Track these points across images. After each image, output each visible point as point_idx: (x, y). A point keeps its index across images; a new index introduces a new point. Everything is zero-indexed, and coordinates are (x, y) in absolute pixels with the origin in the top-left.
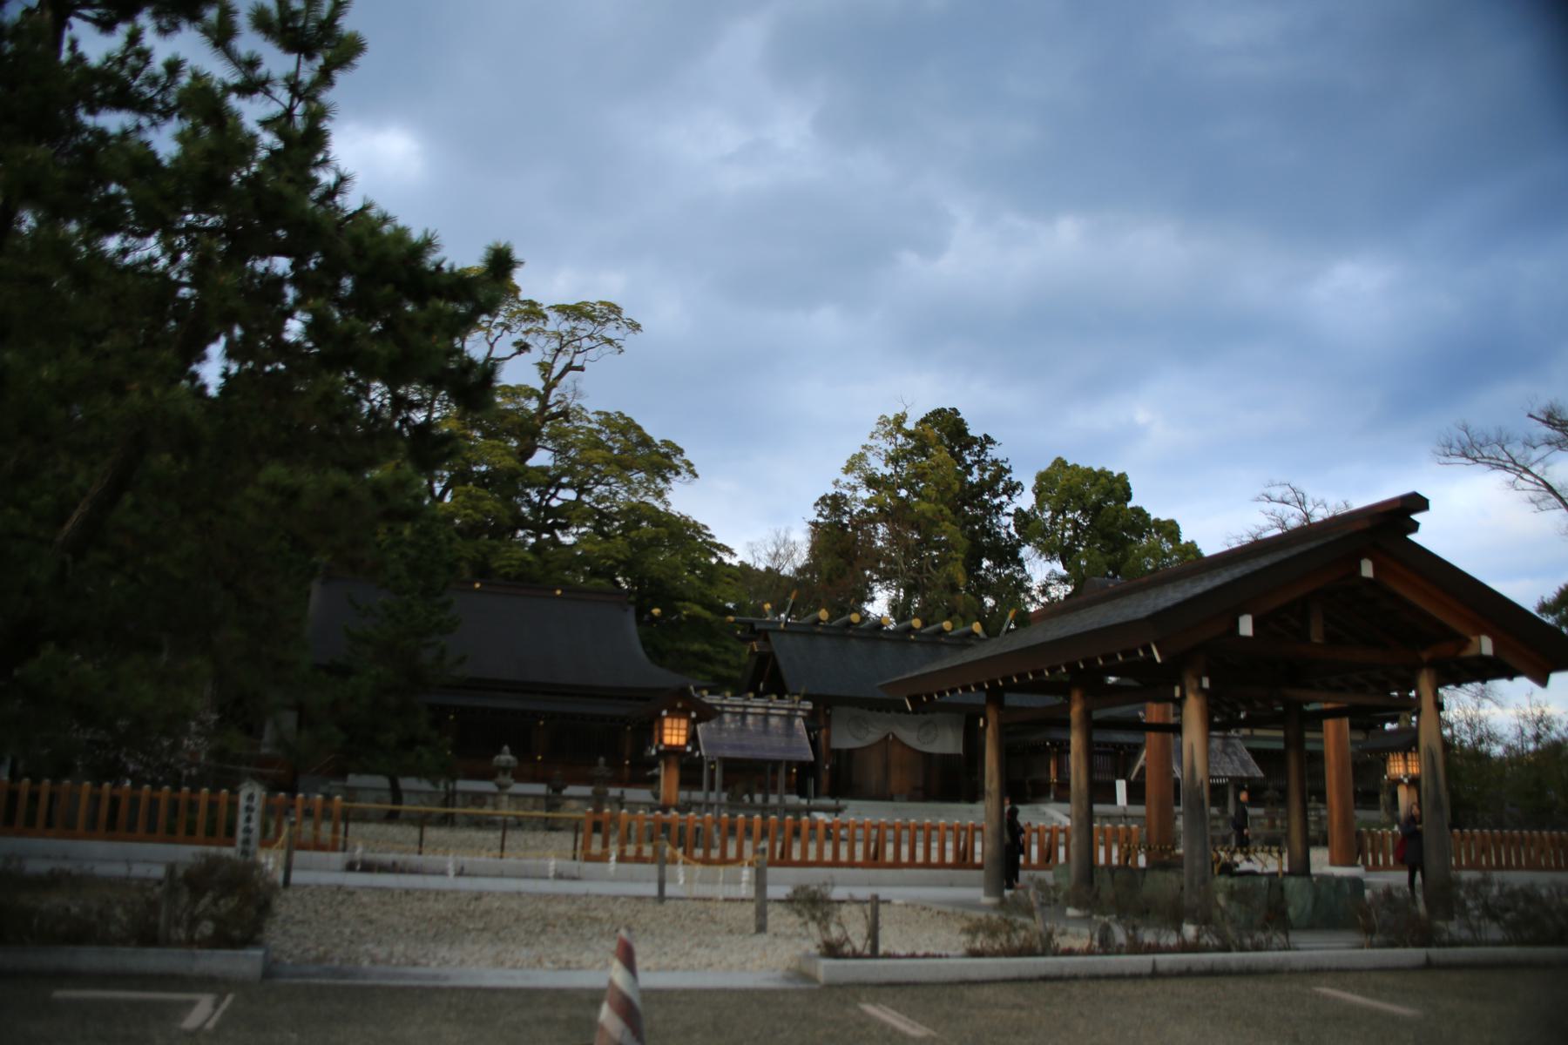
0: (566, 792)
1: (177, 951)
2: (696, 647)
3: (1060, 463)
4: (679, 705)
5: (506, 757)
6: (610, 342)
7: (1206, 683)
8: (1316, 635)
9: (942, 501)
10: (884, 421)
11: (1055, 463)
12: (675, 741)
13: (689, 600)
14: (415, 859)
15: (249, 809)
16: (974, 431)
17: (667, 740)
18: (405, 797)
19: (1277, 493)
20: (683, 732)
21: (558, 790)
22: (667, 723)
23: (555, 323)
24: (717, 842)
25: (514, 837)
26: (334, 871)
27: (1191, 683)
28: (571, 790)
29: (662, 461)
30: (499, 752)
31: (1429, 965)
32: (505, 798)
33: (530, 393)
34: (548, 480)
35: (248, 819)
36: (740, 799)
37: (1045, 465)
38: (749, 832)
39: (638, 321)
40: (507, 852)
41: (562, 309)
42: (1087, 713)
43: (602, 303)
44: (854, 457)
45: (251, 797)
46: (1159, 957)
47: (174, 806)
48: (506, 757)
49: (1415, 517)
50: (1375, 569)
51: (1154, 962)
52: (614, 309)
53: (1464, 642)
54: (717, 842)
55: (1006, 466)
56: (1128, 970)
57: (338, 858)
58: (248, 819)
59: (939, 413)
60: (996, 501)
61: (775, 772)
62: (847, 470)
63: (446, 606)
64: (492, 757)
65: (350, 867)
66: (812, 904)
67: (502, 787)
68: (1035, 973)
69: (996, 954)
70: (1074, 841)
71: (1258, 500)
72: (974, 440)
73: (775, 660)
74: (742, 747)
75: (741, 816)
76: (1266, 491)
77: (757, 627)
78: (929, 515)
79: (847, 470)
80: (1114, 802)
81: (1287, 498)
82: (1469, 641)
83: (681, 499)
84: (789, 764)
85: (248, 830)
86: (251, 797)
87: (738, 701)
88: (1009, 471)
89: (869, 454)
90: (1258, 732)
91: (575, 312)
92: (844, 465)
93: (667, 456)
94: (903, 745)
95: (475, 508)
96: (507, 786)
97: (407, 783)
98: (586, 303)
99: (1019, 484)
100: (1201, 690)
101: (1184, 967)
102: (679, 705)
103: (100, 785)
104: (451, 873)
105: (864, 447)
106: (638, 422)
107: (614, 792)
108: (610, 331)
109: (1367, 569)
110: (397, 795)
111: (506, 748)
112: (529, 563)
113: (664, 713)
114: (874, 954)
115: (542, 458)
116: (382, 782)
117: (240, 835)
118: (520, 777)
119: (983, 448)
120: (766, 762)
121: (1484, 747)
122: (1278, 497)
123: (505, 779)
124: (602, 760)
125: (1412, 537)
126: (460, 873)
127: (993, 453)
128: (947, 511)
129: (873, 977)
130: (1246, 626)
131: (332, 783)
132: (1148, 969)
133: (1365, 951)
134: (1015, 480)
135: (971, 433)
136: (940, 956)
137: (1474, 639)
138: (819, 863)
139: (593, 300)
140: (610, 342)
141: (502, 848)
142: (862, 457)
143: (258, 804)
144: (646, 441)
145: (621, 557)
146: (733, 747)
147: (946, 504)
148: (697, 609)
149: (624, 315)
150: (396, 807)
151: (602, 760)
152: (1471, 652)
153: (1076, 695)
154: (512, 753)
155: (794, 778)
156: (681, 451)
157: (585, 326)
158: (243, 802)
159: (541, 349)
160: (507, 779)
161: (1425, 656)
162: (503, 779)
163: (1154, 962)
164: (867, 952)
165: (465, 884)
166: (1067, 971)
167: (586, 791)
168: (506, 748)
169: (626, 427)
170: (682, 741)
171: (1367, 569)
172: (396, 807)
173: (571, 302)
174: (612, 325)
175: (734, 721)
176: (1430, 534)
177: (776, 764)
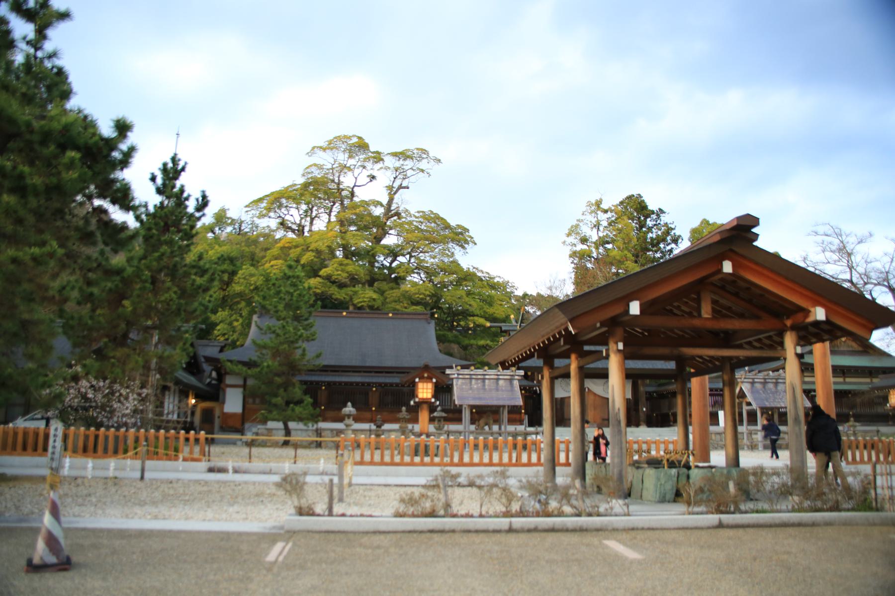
2: (482, 343)
3: (705, 222)
4: (426, 375)
5: (349, 409)
6: (423, 171)
7: (621, 346)
8: (706, 311)
9: (627, 248)
10: (590, 204)
11: (702, 223)
12: (425, 396)
13: (477, 316)
14: (246, 465)
15: (55, 436)
16: (652, 206)
17: (421, 395)
18: (293, 433)
19: (821, 230)
20: (430, 391)
21: (379, 426)
22: (420, 385)
23: (390, 161)
24: (449, 452)
25: (300, 452)
26: (201, 472)
27: (612, 346)
28: (386, 426)
29: (460, 237)
30: (345, 406)
31: (721, 525)
32: (350, 432)
33: (378, 203)
34: (393, 253)
35: (55, 441)
36: (483, 428)
37: (696, 224)
38: (476, 446)
39: (439, 158)
40: (253, 459)
41: (395, 155)
42: (581, 368)
43: (417, 149)
44: (572, 227)
45: (56, 430)
46: (514, 520)
47: (117, 438)
48: (349, 409)
49: (754, 230)
50: (734, 266)
51: (511, 523)
52: (424, 151)
53: (807, 312)
54: (449, 452)
55: (673, 226)
56: (491, 528)
57: (203, 465)
58: (55, 441)
59: (630, 197)
60: (668, 248)
62: (569, 235)
63: (311, 326)
64: (341, 409)
65: (211, 470)
66: (292, 484)
67: (347, 426)
68: (425, 528)
69: (413, 516)
70: (571, 447)
71: (809, 235)
72: (653, 212)
74: (480, 399)
75: (481, 438)
76: (814, 229)
77: (503, 329)
78: (618, 258)
79: (569, 235)
80: (718, 424)
81: (829, 233)
82: (810, 311)
83: (466, 259)
85: (54, 447)
86: (56, 430)
87: (480, 372)
88: (673, 229)
89: (581, 224)
90: (848, 380)
91: (403, 155)
92: (567, 232)
93: (461, 233)
94: (595, 394)
95: (343, 271)
96: (350, 425)
97: (292, 425)
98: (408, 150)
99: (679, 236)
100: (619, 351)
101: (532, 526)
102: (426, 375)
103: (79, 429)
104: (231, 471)
105: (578, 220)
106: (441, 215)
107: (410, 426)
108: (423, 165)
109: (727, 267)
110: (288, 432)
111: (349, 404)
112: (374, 300)
114: (331, 514)
115: (390, 240)
116: (280, 425)
117: (50, 449)
118: (357, 419)
119: (658, 216)
121: (184, 366)
122: (822, 233)
125: (755, 244)
126: (236, 471)
127: (664, 219)
128: (629, 255)
129: (317, 528)
130: (635, 308)
131: (259, 427)
132: (506, 527)
133: (686, 517)
134: (677, 234)
135: (650, 208)
136: (371, 516)
137: (812, 309)
138: (481, 464)
139: (412, 148)
140: (423, 171)
141: (250, 458)
142: (577, 226)
143: (60, 433)
144: (447, 226)
145: (427, 293)
146: (474, 399)
147: (629, 251)
148: (481, 321)
149: (431, 155)
150: (287, 438)
152: (810, 319)
153: (573, 357)
154: (353, 406)
156: (468, 231)
157: (409, 164)
158: (52, 432)
159: (385, 178)
160: (350, 421)
161: (789, 323)
162: (347, 421)
163: (511, 523)
164: (327, 513)
165: (238, 477)
166: (447, 527)
167: (396, 426)
168: (349, 404)
169: (436, 218)
170: (429, 396)
171: (727, 267)
172: (287, 438)
173: (400, 150)
174: (425, 161)
175: (477, 384)
176: (767, 240)
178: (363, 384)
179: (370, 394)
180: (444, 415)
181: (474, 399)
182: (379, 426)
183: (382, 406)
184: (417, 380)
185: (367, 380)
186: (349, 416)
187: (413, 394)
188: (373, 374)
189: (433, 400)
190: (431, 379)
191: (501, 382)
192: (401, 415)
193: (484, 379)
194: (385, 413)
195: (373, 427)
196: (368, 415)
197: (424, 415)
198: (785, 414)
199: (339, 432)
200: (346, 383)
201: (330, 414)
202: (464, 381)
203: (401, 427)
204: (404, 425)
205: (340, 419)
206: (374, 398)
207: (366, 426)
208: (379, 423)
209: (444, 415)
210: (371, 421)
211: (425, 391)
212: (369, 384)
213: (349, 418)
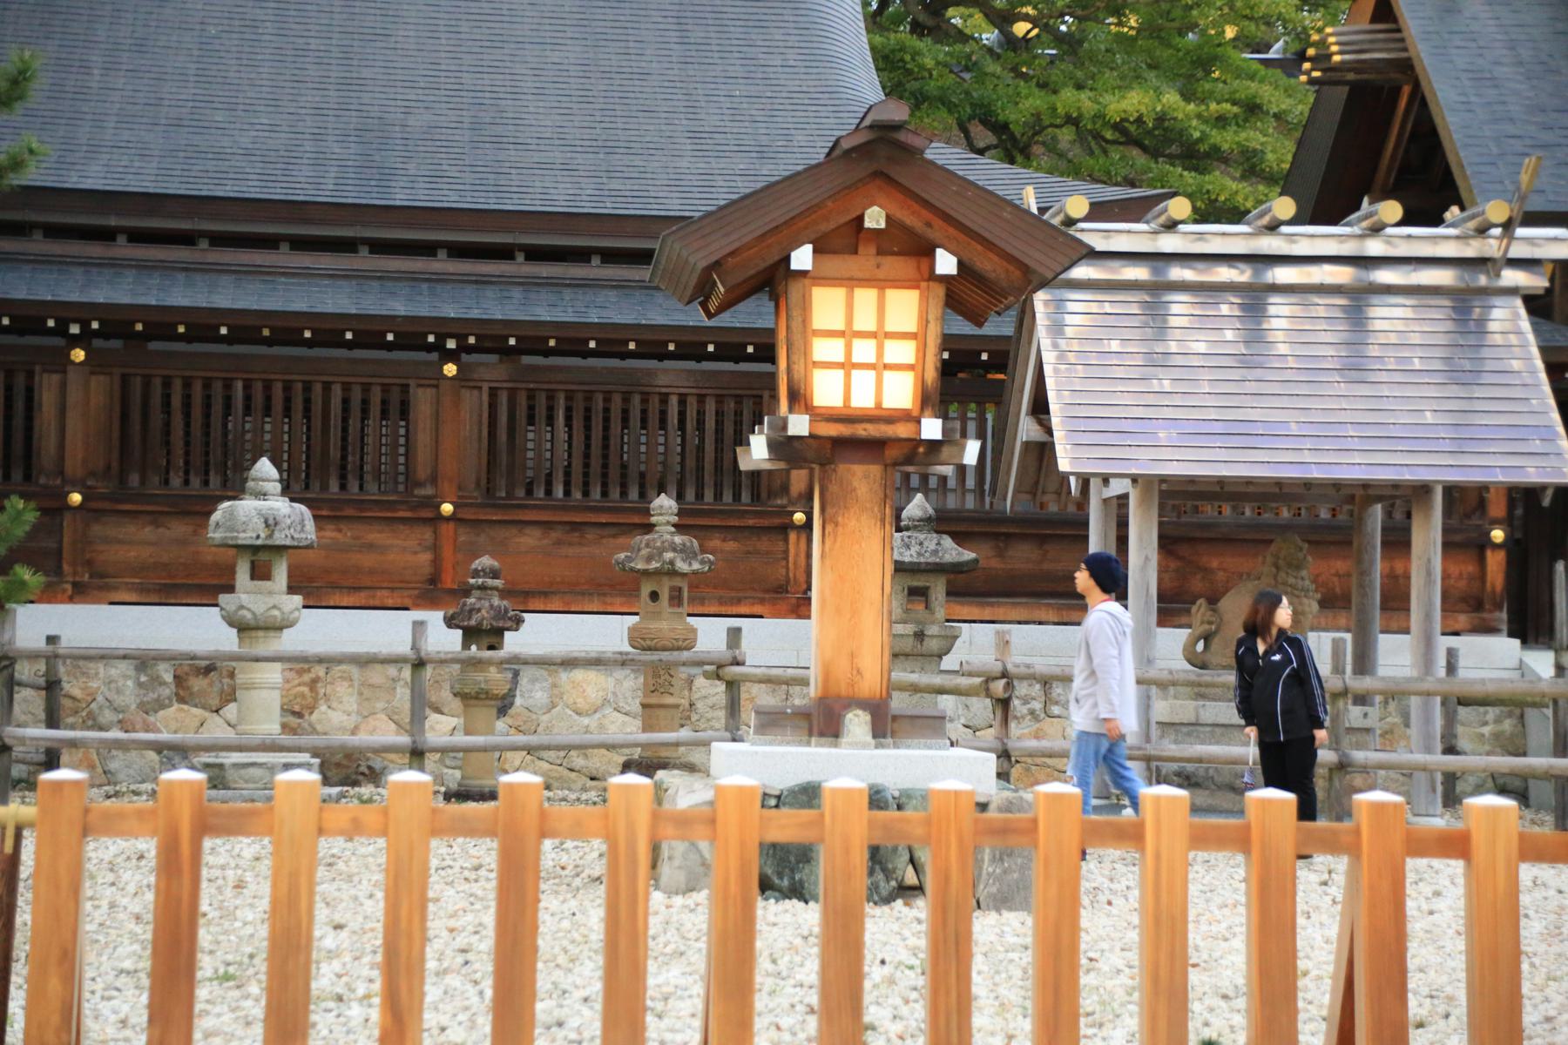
0: (513, 642)
1: (676, 772)
2: (1133, 102)
4: (875, 218)
5: (264, 506)
17: (826, 391)
21: (484, 634)
28: (539, 633)
30: (236, 487)
48: (264, 506)
61: (1398, 541)
64: (201, 510)
73: (1420, 101)
74: (1241, 434)
84: (1465, 503)
107: (710, 634)
111: (265, 467)
113: (802, 258)
118: (320, 585)
120: (1358, 495)
123: (268, 596)
124: (664, 505)
151: (664, 505)
155: (1496, 563)
162: (249, 597)
167: (606, 632)
168: (265, 467)
170: (900, 393)
175: (1203, 323)
177: (1403, 500)
178: (370, 333)
179: (423, 400)
180: (951, 551)
181: (1200, 434)
182: (484, 634)
183: (503, 489)
184: (802, 258)
185: (400, 305)
186: (261, 558)
187: (749, 372)
188: (441, 264)
189: (932, 428)
190: (926, 252)
191: (1388, 316)
192: (636, 554)
193: (1255, 298)
194: (530, 539)
195: (443, 638)
196: (405, 550)
197: (855, 558)
198: (671, 598)
199: (200, 679)
200: (246, 327)
201: (134, 541)
202: (1108, 304)
203: (635, 637)
204: (666, 624)
205: (200, 583)
206: (448, 422)
207: (384, 631)
208: (485, 608)
209: (951, 551)
210: (429, 591)
211: (861, 349)
212: (411, 335)
213: (260, 573)
